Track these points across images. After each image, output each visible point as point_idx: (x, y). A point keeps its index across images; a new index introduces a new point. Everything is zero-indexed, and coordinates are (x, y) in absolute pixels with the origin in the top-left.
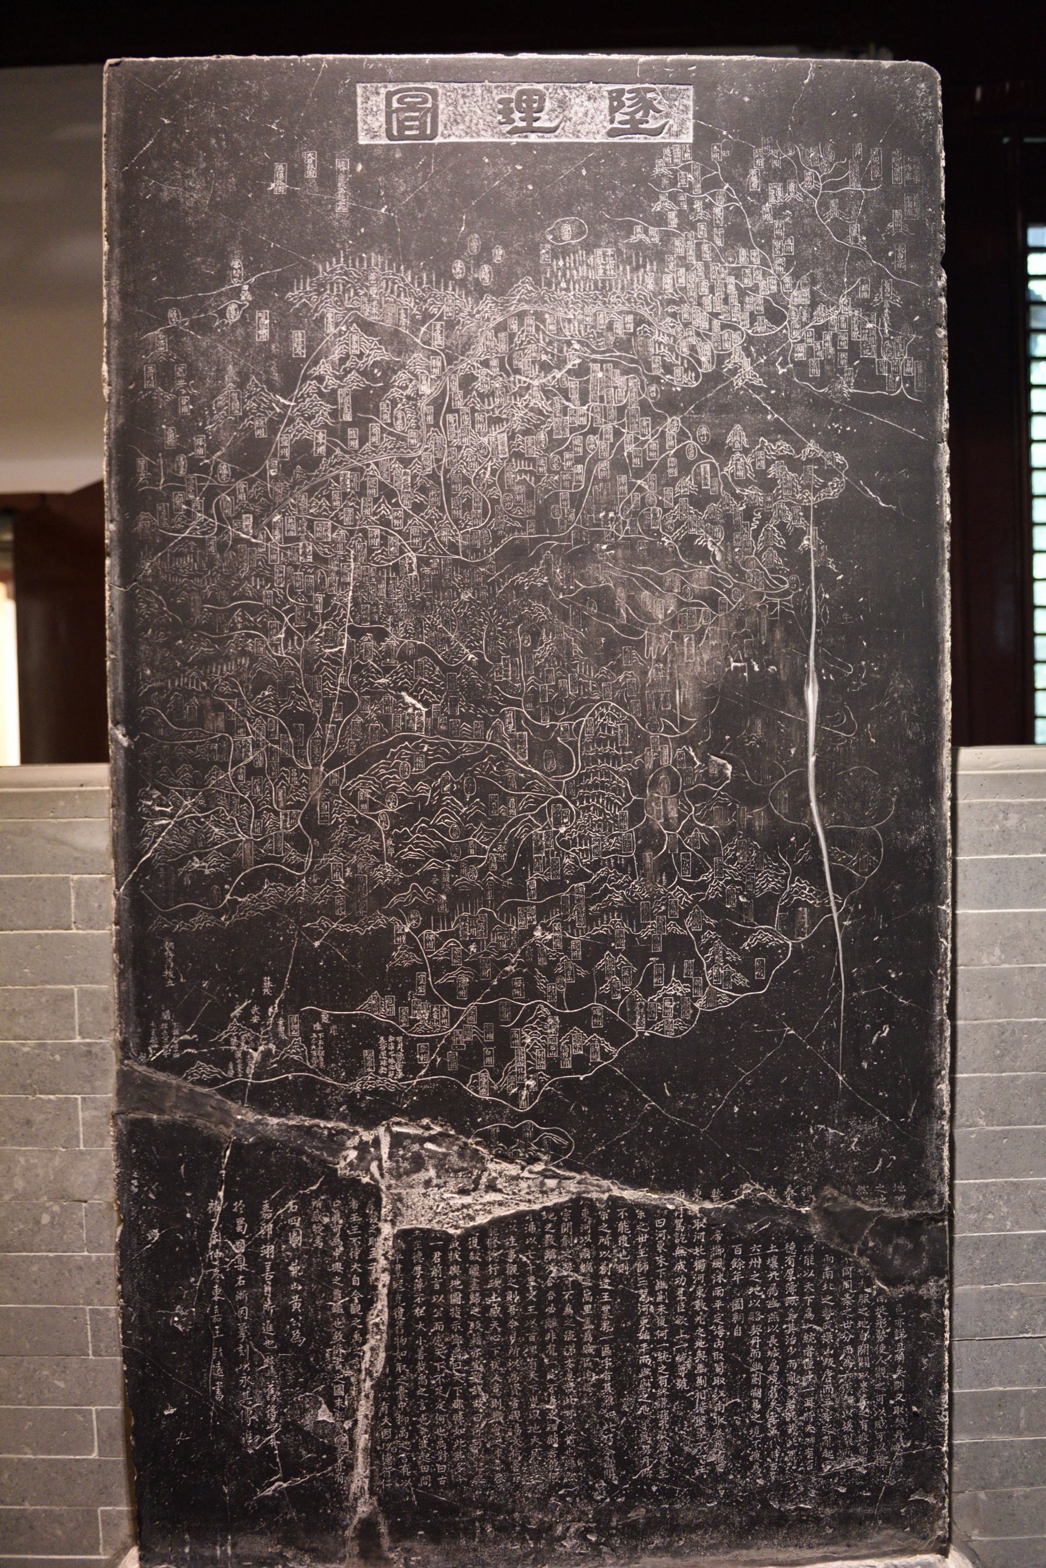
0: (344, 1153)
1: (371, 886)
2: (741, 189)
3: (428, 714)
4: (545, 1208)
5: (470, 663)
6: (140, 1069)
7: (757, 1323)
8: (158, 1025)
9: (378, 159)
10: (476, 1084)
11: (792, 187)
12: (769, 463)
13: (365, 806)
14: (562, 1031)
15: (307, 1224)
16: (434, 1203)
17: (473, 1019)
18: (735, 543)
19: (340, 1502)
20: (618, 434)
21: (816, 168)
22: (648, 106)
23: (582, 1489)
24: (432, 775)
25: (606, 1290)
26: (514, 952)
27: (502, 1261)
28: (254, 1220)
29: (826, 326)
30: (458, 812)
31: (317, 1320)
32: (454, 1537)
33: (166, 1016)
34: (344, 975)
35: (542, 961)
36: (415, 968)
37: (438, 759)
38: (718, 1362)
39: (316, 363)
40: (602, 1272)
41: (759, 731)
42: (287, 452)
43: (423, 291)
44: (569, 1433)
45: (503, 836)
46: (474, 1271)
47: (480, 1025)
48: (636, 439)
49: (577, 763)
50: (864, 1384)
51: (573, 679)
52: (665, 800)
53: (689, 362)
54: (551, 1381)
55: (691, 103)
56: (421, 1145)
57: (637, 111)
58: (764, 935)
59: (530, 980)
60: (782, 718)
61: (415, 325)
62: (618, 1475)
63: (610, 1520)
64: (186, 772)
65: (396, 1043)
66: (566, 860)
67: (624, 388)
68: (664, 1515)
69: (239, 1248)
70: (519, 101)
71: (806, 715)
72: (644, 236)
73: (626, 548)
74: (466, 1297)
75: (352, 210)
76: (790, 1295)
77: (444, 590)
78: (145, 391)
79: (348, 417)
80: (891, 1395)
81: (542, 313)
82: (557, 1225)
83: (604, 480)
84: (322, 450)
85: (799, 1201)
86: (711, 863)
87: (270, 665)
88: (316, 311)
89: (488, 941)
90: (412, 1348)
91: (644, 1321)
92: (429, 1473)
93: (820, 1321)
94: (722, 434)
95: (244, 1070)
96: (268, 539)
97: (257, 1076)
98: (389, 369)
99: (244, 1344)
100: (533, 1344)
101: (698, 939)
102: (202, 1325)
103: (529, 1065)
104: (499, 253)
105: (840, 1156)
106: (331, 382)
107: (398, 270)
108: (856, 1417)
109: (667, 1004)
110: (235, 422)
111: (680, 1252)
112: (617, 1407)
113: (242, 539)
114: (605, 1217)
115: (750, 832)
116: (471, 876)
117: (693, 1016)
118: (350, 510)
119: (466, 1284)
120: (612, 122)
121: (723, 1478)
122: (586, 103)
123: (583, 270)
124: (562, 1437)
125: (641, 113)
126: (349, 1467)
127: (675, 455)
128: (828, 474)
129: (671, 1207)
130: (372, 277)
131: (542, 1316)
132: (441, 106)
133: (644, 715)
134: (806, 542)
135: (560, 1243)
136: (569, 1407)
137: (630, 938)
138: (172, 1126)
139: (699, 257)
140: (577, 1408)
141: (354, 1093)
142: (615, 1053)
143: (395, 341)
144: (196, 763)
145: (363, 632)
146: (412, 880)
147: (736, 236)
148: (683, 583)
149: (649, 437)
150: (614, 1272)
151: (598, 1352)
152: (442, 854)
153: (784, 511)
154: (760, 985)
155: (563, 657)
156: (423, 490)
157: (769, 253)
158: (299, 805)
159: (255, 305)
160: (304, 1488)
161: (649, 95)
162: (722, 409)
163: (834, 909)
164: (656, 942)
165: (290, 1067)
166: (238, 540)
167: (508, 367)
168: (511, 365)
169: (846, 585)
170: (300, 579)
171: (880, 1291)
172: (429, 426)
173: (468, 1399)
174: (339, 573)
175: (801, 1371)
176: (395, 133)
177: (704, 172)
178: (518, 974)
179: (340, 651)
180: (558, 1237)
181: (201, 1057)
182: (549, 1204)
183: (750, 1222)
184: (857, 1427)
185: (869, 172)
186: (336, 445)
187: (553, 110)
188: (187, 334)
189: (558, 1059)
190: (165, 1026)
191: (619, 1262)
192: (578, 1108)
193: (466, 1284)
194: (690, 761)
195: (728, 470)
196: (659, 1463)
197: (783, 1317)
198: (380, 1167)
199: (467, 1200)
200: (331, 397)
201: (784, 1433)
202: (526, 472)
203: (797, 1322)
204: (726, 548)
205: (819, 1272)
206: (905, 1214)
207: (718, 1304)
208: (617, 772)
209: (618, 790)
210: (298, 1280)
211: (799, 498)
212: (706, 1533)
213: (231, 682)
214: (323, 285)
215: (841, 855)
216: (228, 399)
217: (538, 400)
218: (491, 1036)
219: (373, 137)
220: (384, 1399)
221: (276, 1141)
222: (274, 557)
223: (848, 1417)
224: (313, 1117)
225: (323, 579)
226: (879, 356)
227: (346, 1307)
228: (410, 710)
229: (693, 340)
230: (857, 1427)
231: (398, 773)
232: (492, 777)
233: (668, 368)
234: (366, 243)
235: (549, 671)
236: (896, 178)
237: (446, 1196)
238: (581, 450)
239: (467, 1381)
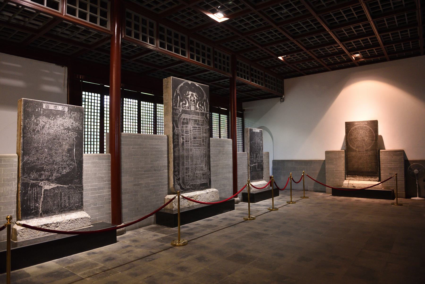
16: (47, 187)
28: (32, 189)
34: (40, 170)
58: (71, 166)
67: (62, 128)
143: (45, 123)
147: (70, 118)
155: (57, 146)
167: (54, 126)
211: (74, 136)
231: (44, 155)
234: (44, 115)
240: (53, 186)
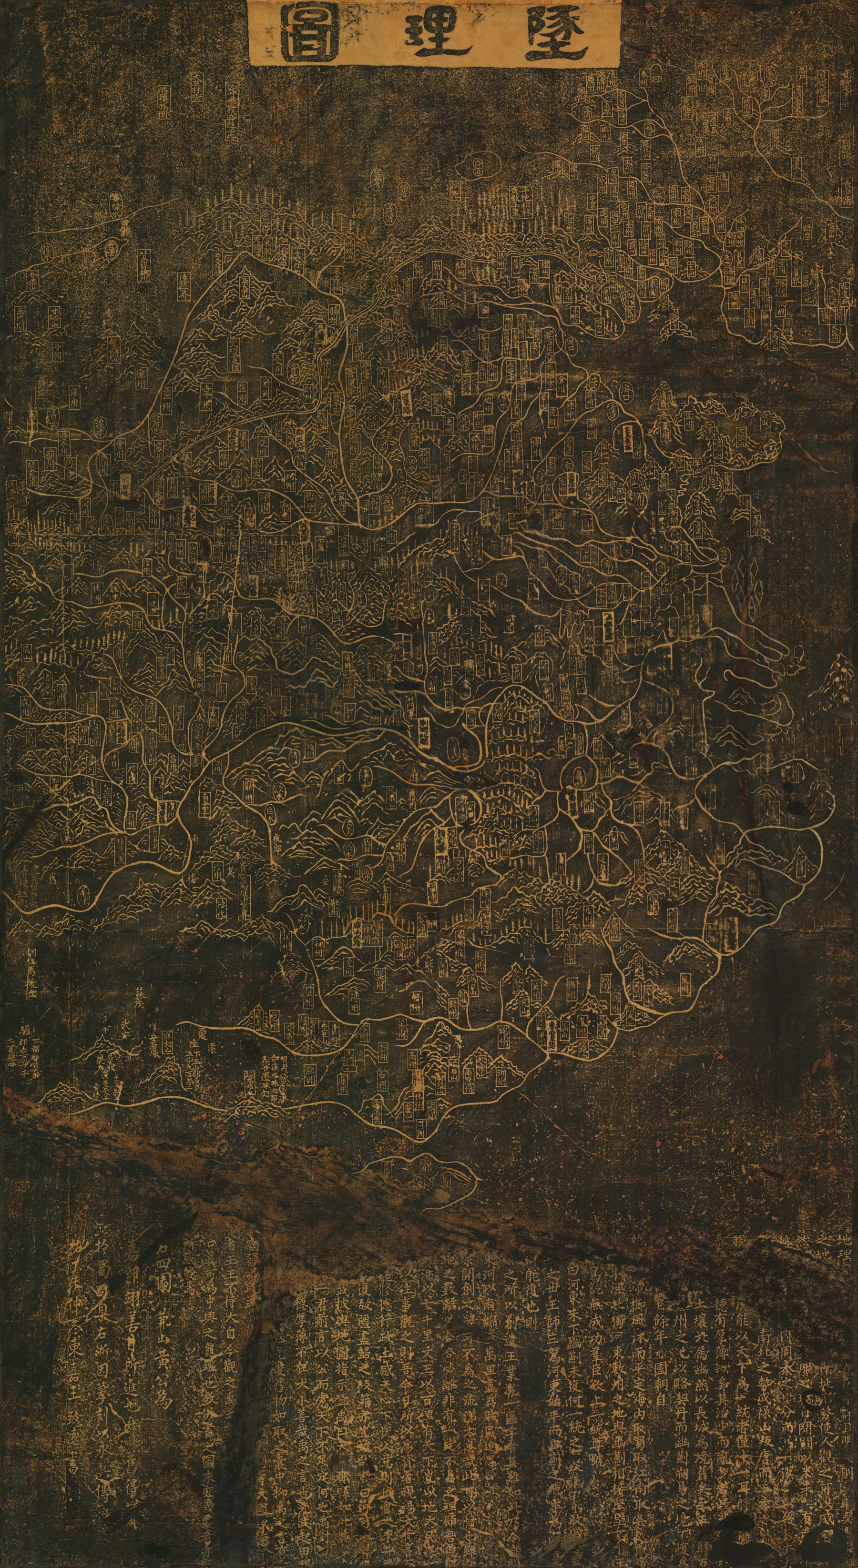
13: (250, 797)
25: (511, 1349)
29: (763, 272)
30: (352, 805)
45: (404, 830)
53: (611, 312)
65: (280, 1063)
74: (354, 1350)
91: (555, 1384)
117: (611, 1035)
119: (355, 1336)
125: (562, 34)
132: (342, 23)
136: (469, 1483)
142: (524, 1075)
146: (301, 881)
174: (226, 539)
176: (291, 52)
202: (431, 433)
226: (822, 304)
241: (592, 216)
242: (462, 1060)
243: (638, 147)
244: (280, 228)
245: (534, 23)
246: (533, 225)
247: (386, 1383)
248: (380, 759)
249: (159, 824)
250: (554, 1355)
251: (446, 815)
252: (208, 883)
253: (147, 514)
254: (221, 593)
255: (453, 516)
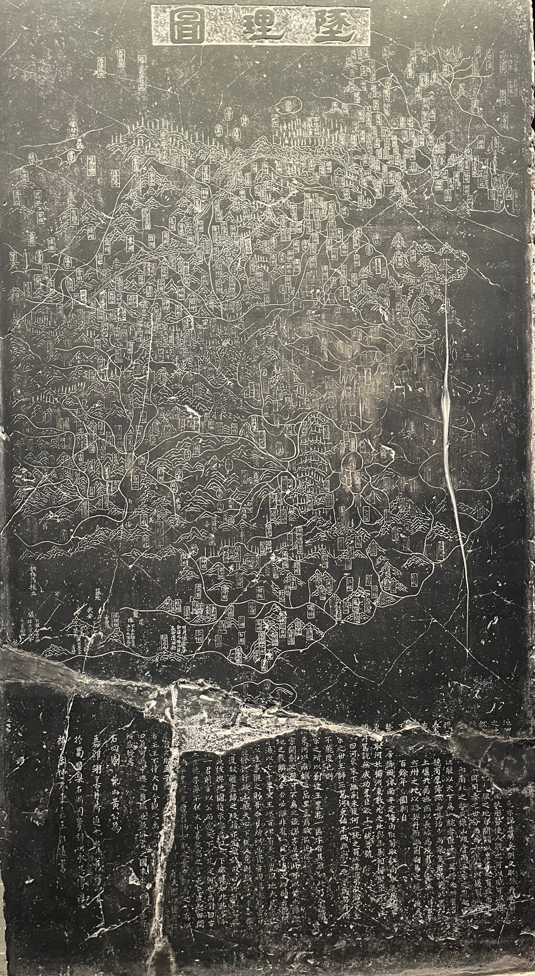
0: (148, 703)
1: (166, 529)
2: (401, 77)
3: (202, 419)
4: (278, 737)
5: (228, 387)
6: (14, 650)
7: (416, 813)
8: (25, 622)
9: (165, 55)
10: (234, 656)
11: (434, 76)
12: (418, 258)
14: (289, 621)
15: (123, 751)
17: (232, 613)
18: (397, 309)
19: (143, 941)
20: (322, 239)
21: (450, 63)
22: (341, 22)
23: (304, 928)
24: (206, 457)
25: (318, 791)
26: (258, 570)
27: (251, 772)
28: (88, 748)
29: (456, 168)
30: (222, 482)
31: (129, 815)
32: (220, 962)
33: (31, 615)
35: (276, 576)
36: (195, 581)
37: (209, 448)
38: (392, 839)
39: (126, 191)
40: (316, 779)
41: (412, 430)
42: (109, 250)
43: (196, 144)
44: (295, 888)
45: (250, 496)
46: (232, 779)
47: (236, 617)
48: (334, 242)
49: (297, 449)
50: (488, 855)
51: (294, 397)
52: (352, 473)
54: (283, 853)
55: (369, 20)
56: (198, 697)
57: (334, 25)
58: (419, 558)
59: (267, 587)
60: (427, 421)
61: (191, 166)
62: (327, 917)
63: (323, 949)
64: (44, 456)
65: (182, 630)
66: (290, 512)
68: (358, 945)
69: (78, 767)
70: (257, 18)
71: (442, 419)
72: (338, 109)
73: (327, 313)
74: (227, 797)
75: (149, 89)
76: (437, 793)
77: (211, 339)
78: (14, 207)
79: (148, 227)
80: (506, 862)
81: (274, 160)
82: (286, 748)
83: (313, 269)
84: (132, 248)
85: (442, 731)
86: (382, 513)
87: (99, 387)
88: (126, 157)
89: (241, 563)
90: (192, 832)
92: (203, 918)
93: (458, 811)
94: (388, 239)
95: (82, 649)
96: (97, 306)
97: (91, 653)
98: (175, 196)
99: (80, 833)
100: (271, 827)
101: (375, 562)
102: (51, 822)
103: (267, 643)
104: (245, 120)
105: (469, 702)
106: (137, 204)
107: (180, 130)
108: (483, 878)
109: (355, 603)
110: (75, 229)
111: (366, 765)
112: (326, 870)
113: (80, 306)
114: (317, 742)
115: (407, 493)
116: (231, 521)
117: (372, 610)
118: (150, 288)
119: (227, 788)
120: (318, 32)
121: (396, 919)
122: (301, 19)
123: (299, 132)
124: (290, 891)
126: (150, 915)
127: (359, 253)
128: (456, 264)
129: (360, 735)
130: (163, 135)
131: (277, 809)
132: (207, 21)
133: (339, 419)
134: (442, 308)
135: (288, 760)
136: (295, 870)
137: (331, 561)
138: (34, 687)
139: (374, 123)
140: (300, 871)
141: (155, 663)
142: (322, 634)
143: (178, 176)
144: (51, 451)
145: (160, 366)
146: (192, 525)
147: (398, 108)
148: (364, 335)
149: (342, 241)
150: (323, 778)
151: (313, 832)
152: (211, 508)
153: (428, 288)
154: (415, 591)
155: (288, 383)
156: (198, 275)
157: (419, 120)
158: (119, 477)
159: (86, 152)
160: (119, 932)
161: (342, 14)
162: (388, 222)
163: (461, 542)
164: (348, 563)
165: (112, 647)
166: (77, 307)
168: (253, 193)
169: (467, 335)
170: (119, 333)
171: (497, 792)
172: (201, 234)
173: (229, 866)
175: (446, 846)
176: (176, 38)
177: (377, 66)
178: (261, 584)
179: (145, 378)
180: (287, 755)
181: (54, 641)
182: (281, 734)
183: (411, 745)
184: (484, 884)
185: (485, 65)
186: (141, 245)
187: (279, 24)
188: (41, 171)
189: (286, 639)
190: (30, 621)
191: (326, 772)
192: (299, 671)
193: (227, 788)
194: (368, 448)
195: (393, 261)
196: (354, 909)
197: (433, 808)
198: (171, 712)
199: (228, 732)
200: (138, 214)
201: (436, 888)
202: (263, 264)
203: (443, 812)
204: (391, 312)
205: (456, 779)
206: (511, 740)
207: (391, 800)
208: (322, 456)
209: (322, 467)
210: (117, 788)
212: (386, 957)
213: (73, 398)
214: (131, 140)
215: (465, 508)
216: (71, 216)
217: (269, 215)
218: (243, 624)
219: (162, 41)
220: (173, 868)
221: (103, 695)
222: (101, 318)
223: (478, 877)
224: (127, 679)
225: (133, 333)
226: (490, 187)
227: (148, 805)
228: (191, 417)
229: (370, 178)
230: (484, 884)
232: (243, 459)
233: (354, 197)
234: (158, 113)
235: (279, 392)
236: (502, 69)
237: (213, 730)
238: (298, 249)
239: (228, 853)
240: (267, 723)
241: (355, 136)
242: (287, 625)
243: (382, 94)
244: (172, 143)
245: (320, 20)
246: (321, 141)
247: (246, 814)
248: (237, 454)
249: (108, 494)
250: (343, 795)
251: (275, 486)
252: (138, 527)
253: (96, 313)
254: (141, 359)
255: (277, 312)
